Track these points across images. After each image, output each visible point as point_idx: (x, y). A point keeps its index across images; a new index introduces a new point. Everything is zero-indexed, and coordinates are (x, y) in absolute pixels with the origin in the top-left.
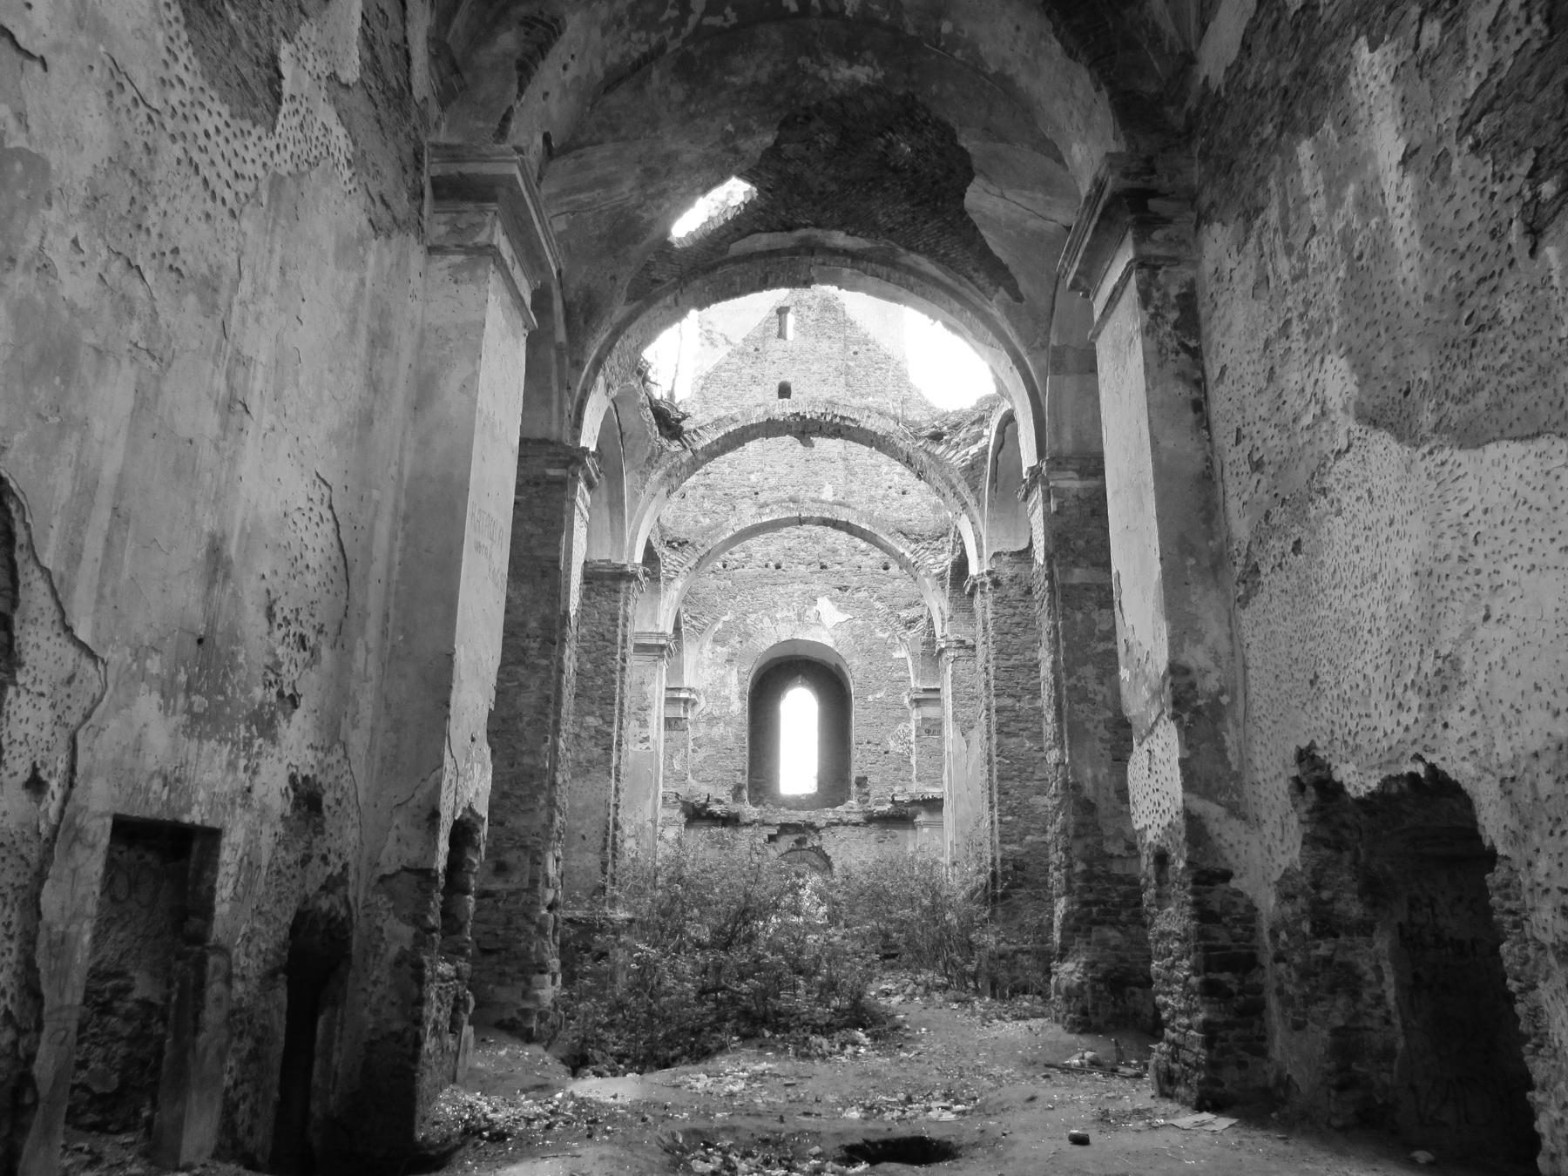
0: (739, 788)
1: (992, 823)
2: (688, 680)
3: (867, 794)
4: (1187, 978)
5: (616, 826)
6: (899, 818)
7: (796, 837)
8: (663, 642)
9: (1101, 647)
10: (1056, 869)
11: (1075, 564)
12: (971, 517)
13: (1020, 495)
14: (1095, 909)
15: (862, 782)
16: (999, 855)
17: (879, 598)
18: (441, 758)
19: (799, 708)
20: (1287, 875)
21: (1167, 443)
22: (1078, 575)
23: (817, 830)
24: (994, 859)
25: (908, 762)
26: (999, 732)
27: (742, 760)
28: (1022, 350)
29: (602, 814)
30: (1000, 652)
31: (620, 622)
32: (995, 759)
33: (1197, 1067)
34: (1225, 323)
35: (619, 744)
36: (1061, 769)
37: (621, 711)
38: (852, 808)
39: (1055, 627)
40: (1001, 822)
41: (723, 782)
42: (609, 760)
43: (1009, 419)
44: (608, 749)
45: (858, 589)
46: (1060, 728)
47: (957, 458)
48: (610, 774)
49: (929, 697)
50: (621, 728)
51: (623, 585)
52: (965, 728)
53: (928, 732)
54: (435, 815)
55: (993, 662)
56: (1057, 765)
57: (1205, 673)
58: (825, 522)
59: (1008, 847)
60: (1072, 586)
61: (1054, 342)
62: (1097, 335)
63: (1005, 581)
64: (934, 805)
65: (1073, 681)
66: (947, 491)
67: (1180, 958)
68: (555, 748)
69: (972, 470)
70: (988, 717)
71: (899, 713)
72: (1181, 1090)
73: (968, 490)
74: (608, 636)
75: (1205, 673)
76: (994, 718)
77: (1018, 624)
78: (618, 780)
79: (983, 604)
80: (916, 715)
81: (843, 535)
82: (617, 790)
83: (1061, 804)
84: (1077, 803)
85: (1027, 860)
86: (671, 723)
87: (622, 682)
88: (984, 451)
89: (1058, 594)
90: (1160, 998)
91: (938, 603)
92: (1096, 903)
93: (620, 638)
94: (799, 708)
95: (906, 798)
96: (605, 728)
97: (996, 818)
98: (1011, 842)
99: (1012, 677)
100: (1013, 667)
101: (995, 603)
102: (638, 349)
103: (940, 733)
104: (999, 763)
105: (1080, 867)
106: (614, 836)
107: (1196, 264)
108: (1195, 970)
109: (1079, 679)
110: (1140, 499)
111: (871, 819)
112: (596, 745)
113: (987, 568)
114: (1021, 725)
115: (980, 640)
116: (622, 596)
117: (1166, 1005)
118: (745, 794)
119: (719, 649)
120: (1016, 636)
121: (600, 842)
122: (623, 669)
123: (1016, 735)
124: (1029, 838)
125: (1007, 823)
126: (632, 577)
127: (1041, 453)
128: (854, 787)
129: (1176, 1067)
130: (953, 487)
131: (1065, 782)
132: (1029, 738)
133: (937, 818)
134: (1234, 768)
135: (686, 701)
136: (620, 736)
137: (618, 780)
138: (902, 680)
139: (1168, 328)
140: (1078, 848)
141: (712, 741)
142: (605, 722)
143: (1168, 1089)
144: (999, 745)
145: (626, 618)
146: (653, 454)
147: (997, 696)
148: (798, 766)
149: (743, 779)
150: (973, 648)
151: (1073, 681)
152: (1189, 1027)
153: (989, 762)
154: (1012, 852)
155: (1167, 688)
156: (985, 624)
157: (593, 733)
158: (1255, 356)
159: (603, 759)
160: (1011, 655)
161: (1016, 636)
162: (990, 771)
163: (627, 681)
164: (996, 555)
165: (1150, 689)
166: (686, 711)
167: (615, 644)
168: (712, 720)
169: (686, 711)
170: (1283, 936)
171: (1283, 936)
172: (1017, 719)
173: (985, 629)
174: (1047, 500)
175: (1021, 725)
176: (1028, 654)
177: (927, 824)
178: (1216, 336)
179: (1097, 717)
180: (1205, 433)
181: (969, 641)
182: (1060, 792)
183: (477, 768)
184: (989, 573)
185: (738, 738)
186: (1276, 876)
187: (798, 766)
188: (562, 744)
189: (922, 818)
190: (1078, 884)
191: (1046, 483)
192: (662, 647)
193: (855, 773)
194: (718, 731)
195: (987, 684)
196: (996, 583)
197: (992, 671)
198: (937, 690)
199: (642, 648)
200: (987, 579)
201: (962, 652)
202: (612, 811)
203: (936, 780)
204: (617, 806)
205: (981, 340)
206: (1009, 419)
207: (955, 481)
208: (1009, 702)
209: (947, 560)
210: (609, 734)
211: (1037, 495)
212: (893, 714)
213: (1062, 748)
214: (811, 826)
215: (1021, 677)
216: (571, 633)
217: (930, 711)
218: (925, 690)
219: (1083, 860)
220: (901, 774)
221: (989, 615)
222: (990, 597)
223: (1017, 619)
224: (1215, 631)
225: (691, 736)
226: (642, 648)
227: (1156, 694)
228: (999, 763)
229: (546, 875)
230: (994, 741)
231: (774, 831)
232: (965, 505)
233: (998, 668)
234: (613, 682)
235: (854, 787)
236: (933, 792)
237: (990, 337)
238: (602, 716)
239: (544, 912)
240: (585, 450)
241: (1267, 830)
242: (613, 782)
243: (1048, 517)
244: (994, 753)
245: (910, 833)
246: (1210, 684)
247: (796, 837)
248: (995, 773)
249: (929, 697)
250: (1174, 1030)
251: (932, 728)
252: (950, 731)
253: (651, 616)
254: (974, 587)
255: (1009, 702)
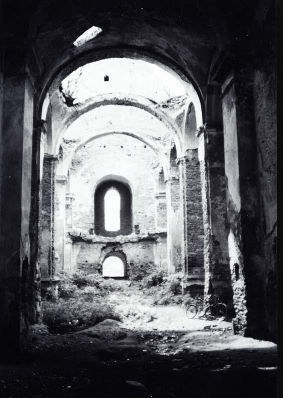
0: (92, 230)
1: (185, 245)
2: (71, 191)
3: (139, 231)
4: (243, 301)
5: (53, 249)
6: (151, 240)
7: (113, 247)
8: (64, 179)
9: (223, 190)
10: (207, 263)
11: (215, 161)
12: (178, 136)
13: (197, 135)
14: (218, 276)
15: (137, 227)
16: (187, 256)
17: (143, 159)
18: (20, 243)
19: (113, 198)
20: (271, 272)
21: (243, 140)
22: (215, 165)
23: (121, 245)
24: (185, 257)
25: (153, 219)
26: (188, 213)
27: (92, 219)
28: (198, 85)
29: (48, 245)
30: (188, 185)
31: (52, 176)
32: (186, 223)
33: (244, 326)
34: (260, 103)
35: (53, 220)
36: (209, 230)
37: (53, 208)
38: (133, 236)
39: (207, 183)
40: (188, 244)
41: (85, 227)
42: (50, 226)
43: (191, 104)
44: (49, 222)
45: (135, 155)
46: (209, 217)
47: (173, 115)
48: (50, 231)
49: (162, 195)
50: (53, 214)
51: (52, 162)
52: (176, 208)
53: (161, 208)
54: (19, 260)
55: (186, 189)
56: (208, 229)
57: (251, 212)
58: (124, 133)
59: (191, 253)
60: (214, 169)
61: (209, 83)
62: (222, 97)
63: (190, 160)
64: (164, 235)
65: (213, 201)
66: (170, 126)
67: (241, 295)
68: (37, 226)
69: (179, 118)
70: (184, 208)
71: (150, 201)
72: (240, 332)
73: (177, 126)
74: (48, 181)
75: (251, 212)
76: (186, 209)
77: (195, 175)
78: (53, 233)
79: (182, 168)
80: (157, 202)
81: (130, 137)
82: (53, 236)
83: (208, 242)
84: (214, 242)
85: (197, 257)
86: (67, 206)
87: (53, 198)
88: (183, 114)
89: (209, 171)
90: (235, 306)
91: (165, 162)
92: (219, 274)
93: (52, 182)
94: (113, 198)
95: (153, 233)
96: (48, 214)
97: (187, 243)
98: (192, 251)
99: (193, 194)
100: (193, 191)
101: (187, 168)
102: (60, 82)
103: (165, 208)
104: (188, 224)
105: (214, 263)
106: (53, 252)
107: (253, 81)
108: (245, 298)
109: (215, 201)
110: (234, 156)
111: (140, 240)
112: (45, 220)
113: (184, 155)
114: (195, 211)
115: (181, 176)
116: (52, 166)
117: (237, 308)
118: (94, 231)
119: (83, 177)
120: (194, 179)
121: (48, 254)
122: (53, 193)
123: (194, 214)
124: (197, 250)
125: (191, 245)
126: (56, 159)
127: (204, 122)
128: (134, 229)
129: (239, 325)
130: (172, 125)
131: (210, 235)
132: (198, 215)
133: (165, 240)
134: (259, 240)
135: (71, 198)
136: (53, 217)
137: (53, 233)
138: (151, 189)
139: (244, 102)
140: (214, 256)
141: (81, 213)
142: (48, 212)
143: (237, 332)
144: (188, 218)
145: (54, 174)
146: (62, 114)
147: (187, 201)
148: (112, 222)
149: (93, 227)
150: (178, 180)
151: (213, 201)
152: (243, 315)
153: (184, 224)
154: (192, 255)
155: (240, 217)
156: (183, 175)
157: (43, 216)
158: (268, 117)
159: (48, 225)
160: (192, 186)
161: (194, 179)
162: (185, 227)
163: (55, 197)
164: (188, 150)
165: (235, 216)
166: (71, 202)
167: (50, 184)
168: (80, 205)
169: (71, 202)
170: (269, 289)
171: (269, 289)
172: (194, 209)
173: (183, 177)
174: (205, 139)
175: (195, 211)
176: (198, 186)
177: (160, 242)
178: (258, 107)
179: (221, 213)
180: (226, 233)
181: (177, 178)
182: (208, 238)
183: (27, 243)
184: (185, 157)
185: (91, 211)
186: (268, 272)
187: (112, 222)
188: (39, 225)
189: (159, 240)
190: (213, 268)
191: (205, 132)
192: (64, 181)
193: (134, 223)
194: (83, 209)
195: (184, 197)
196: (187, 161)
197: (185, 192)
198: (164, 193)
199: (59, 182)
200: (184, 159)
201: (174, 181)
202: (51, 243)
203: (164, 225)
204: (53, 242)
205: (183, 79)
206: (191, 104)
207: (173, 123)
208: (191, 203)
209: (169, 148)
210: (49, 217)
211: (202, 135)
212: (148, 201)
213: (209, 224)
214: (118, 243)
215: (195, 194)
216: (41, 186)
217: (161, 201)
218: (160, 193)
219: (215, 260)
220: (151, 224)
221: (185, 172)
222: (185, 166)
223: (194, 173)
224: (252, 198)
225: (73, 212)
226: (59, 182)
227: (237, 218)
228: (188, 224)
229: (36, 270)
230: (186, 216)
231: (105, 245)
232: (176, 132)
233: (187, 191)
234: (50, 198)
235: (134, 229)
236: (162, 230)
237: (187, 79)
238: (47, 210)
239: (36, 281)
240: (43, 121)
241: (266, 259)
242: (51, 233)
243: (206, 145)
244: (186, 220)
245: (154, 245)
246: (253, 215)
247: (113, 247)
248: (186, 228)
249: (162, 195)
250: (239, 315)
251: (163, 207)
252: (169, 209)
253: (61, 170)
254: (179, 162)
255: (191, 203)
